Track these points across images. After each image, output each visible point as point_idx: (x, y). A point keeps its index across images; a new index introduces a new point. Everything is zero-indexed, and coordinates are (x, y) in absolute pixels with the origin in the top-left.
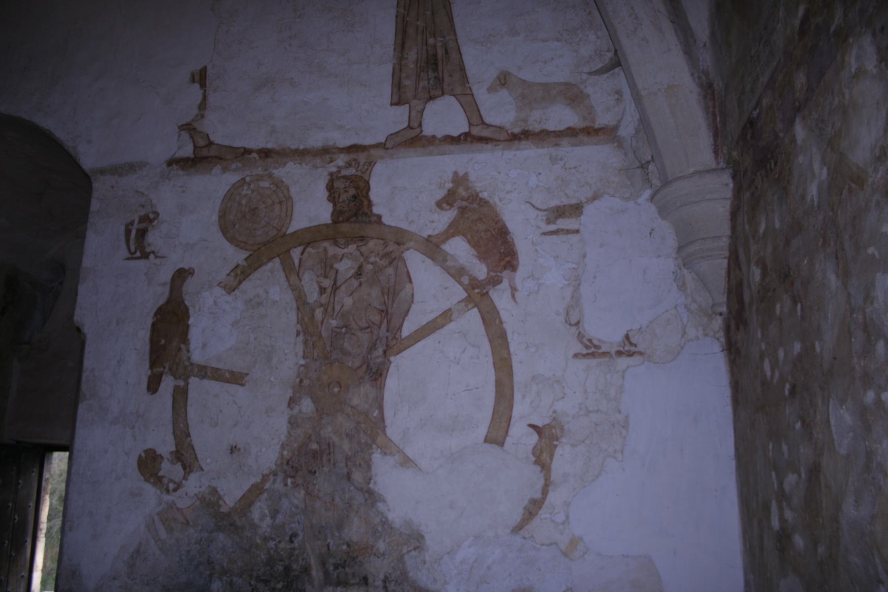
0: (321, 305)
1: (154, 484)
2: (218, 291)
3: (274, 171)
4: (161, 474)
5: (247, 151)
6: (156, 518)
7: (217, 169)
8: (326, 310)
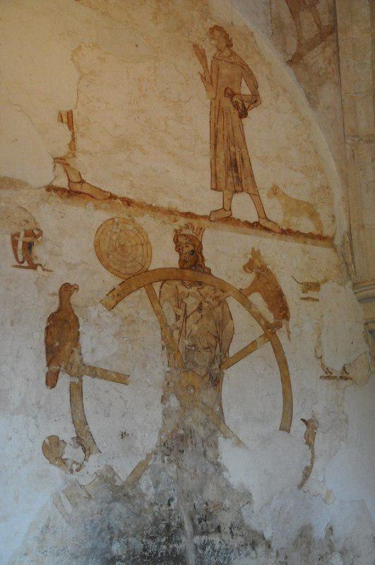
0: (178, 328)
1: (59, 466)
2: (101, 307)
3: (135, 218)
4: (64, 457)
5: (112, 197)
6: (62, 495)
7: (91, 205)
8: (180, 333)
